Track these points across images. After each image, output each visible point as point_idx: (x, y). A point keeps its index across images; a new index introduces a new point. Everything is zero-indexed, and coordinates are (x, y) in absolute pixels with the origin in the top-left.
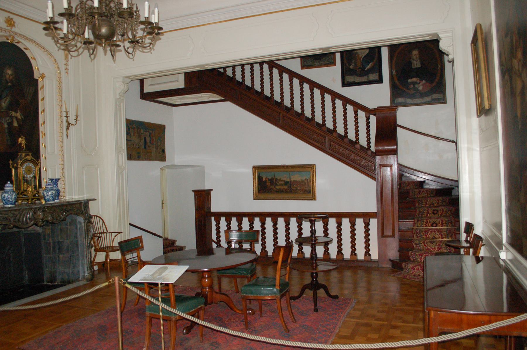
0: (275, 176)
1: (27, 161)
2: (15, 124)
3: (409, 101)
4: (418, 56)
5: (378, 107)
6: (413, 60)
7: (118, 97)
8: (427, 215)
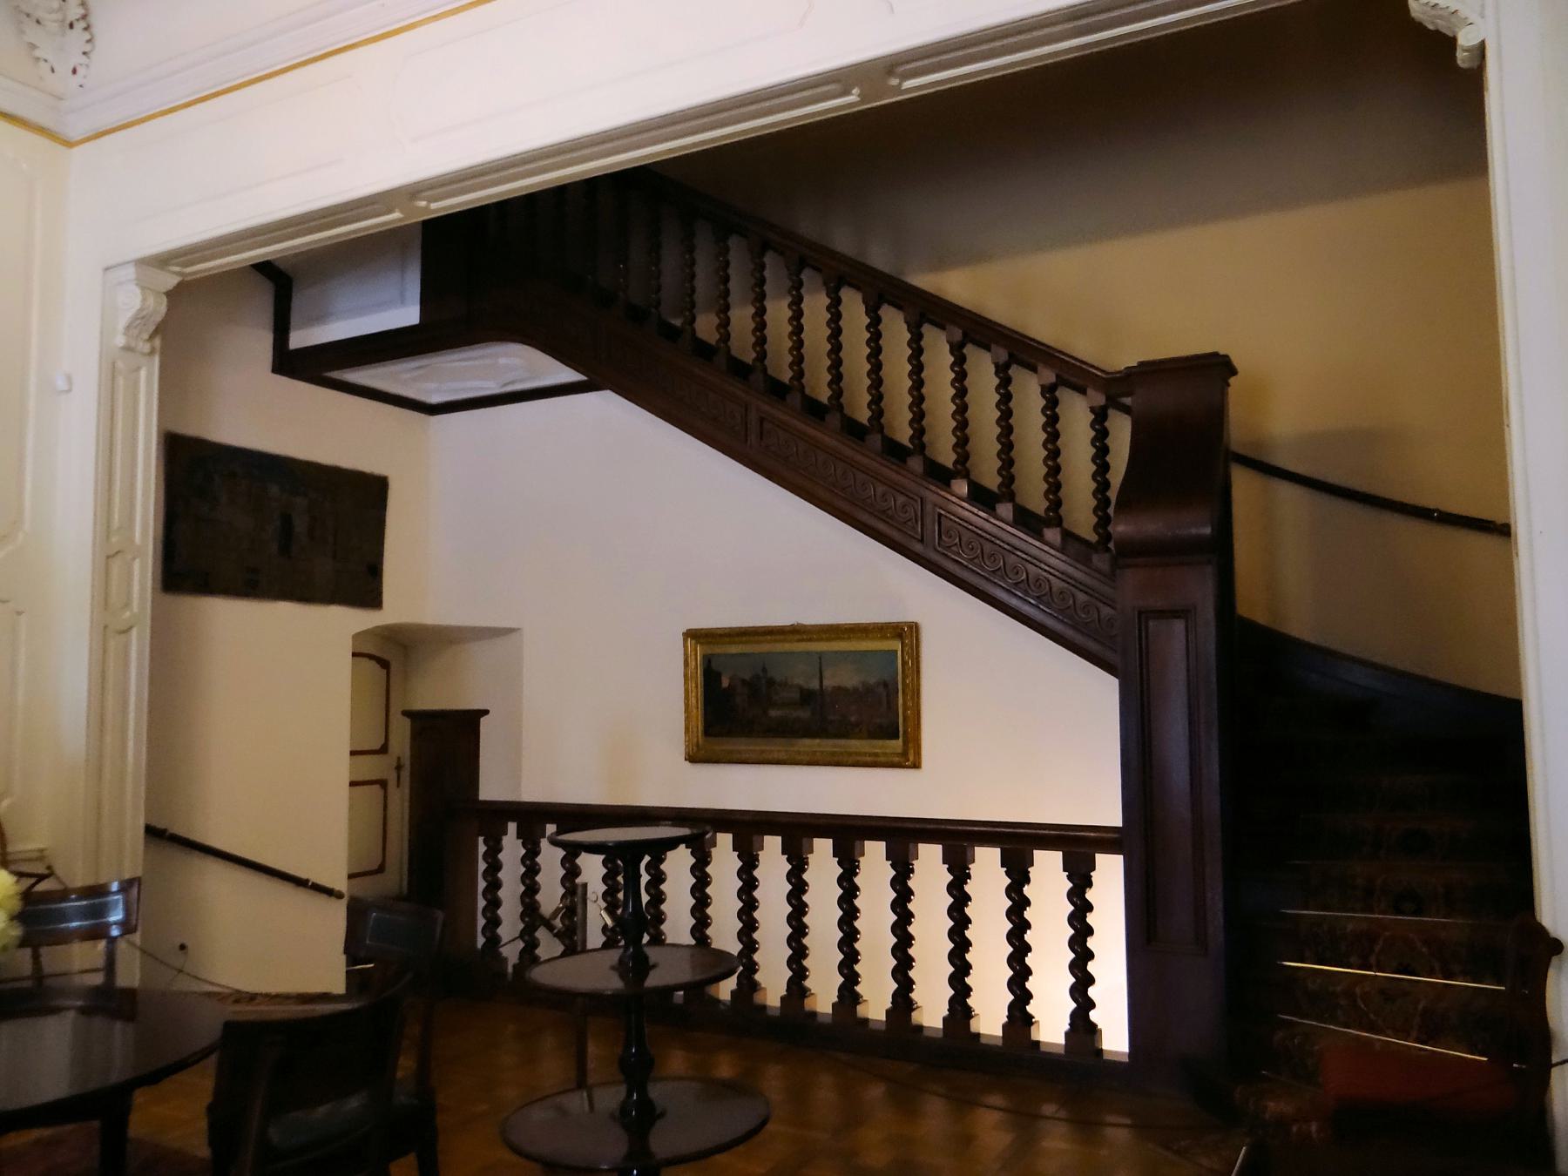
0: (764, 670)
5: (1141, 364)
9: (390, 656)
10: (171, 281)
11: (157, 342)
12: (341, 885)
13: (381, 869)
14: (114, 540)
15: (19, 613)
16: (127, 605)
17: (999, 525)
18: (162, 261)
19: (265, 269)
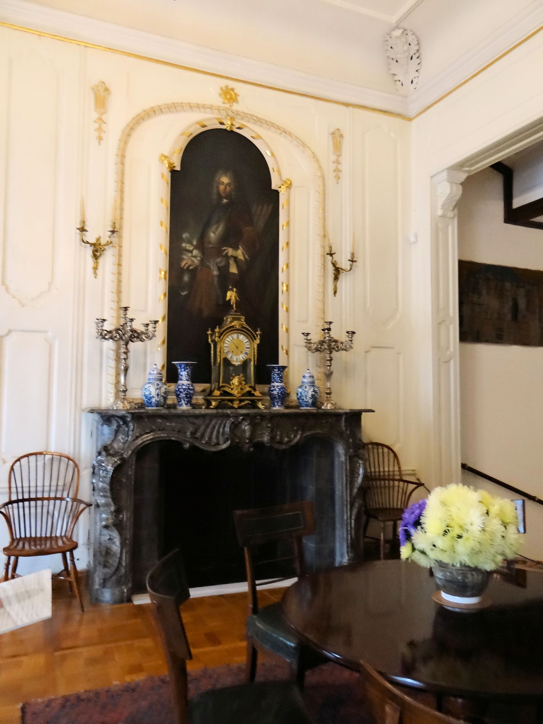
1: (232, 329)
2: (233, 269)
10: (463, 176)
11: (456, 211)
15: (399, 354)
16: (448, 348)
18: (460, 166)
19: (498, 167)
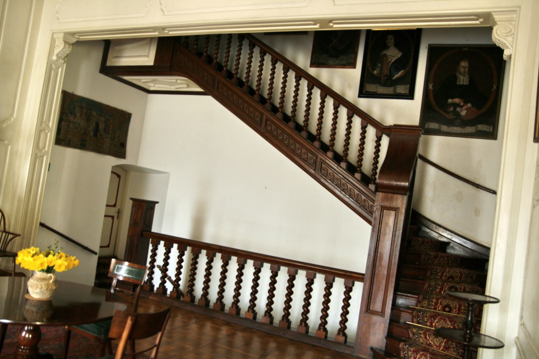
3: (444, 128)
4: (467, 70)
5: (395, 125)
6: (460, 73)
7: (54, 58)
8: (440, 292)
9: (119, 175)
10: (74, 40)
12: (97, 249)
13: (108, 246)
14: (43, 125)
16: (44, 147)
17: (340, 170)
18: (73, 34)
